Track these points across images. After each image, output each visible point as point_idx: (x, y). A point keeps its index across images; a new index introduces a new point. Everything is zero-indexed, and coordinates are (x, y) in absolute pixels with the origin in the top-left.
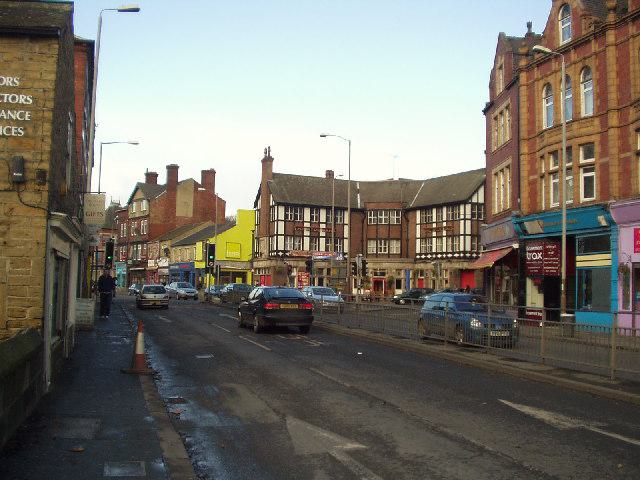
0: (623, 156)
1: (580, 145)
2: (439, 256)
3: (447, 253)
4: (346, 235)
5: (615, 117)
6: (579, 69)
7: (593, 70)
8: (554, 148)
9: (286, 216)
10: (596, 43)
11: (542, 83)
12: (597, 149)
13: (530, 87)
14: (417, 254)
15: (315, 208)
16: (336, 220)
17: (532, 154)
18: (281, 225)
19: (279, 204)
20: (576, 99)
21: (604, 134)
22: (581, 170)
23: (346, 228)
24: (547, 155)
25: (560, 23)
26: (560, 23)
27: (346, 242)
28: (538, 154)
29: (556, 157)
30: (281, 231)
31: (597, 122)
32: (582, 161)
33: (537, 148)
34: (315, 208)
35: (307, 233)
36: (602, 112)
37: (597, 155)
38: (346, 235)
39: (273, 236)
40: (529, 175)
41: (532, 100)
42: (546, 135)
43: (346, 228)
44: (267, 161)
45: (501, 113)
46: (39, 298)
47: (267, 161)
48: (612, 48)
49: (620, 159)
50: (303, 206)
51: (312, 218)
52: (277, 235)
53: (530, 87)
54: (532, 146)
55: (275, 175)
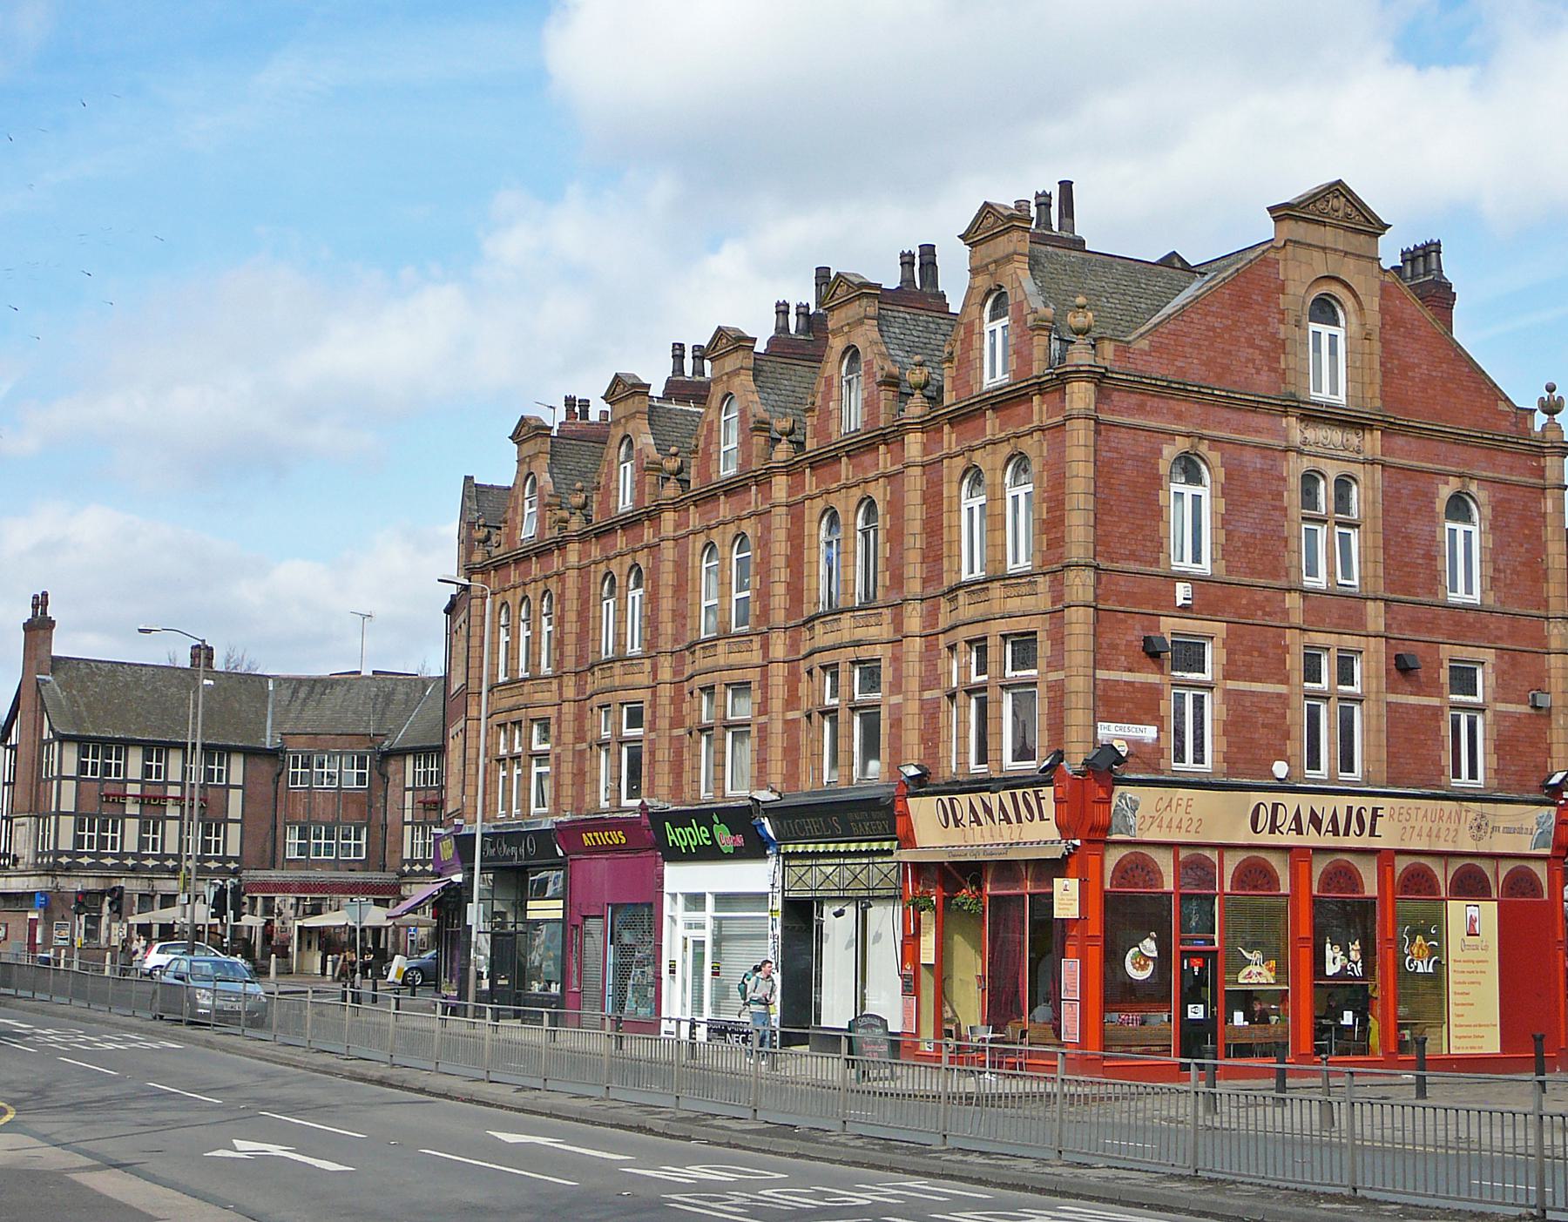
0: (927, 695)
1: (1004, 637)
2: (418, 868)
3: (424, 862)
4: (235, 810)
5: (572, 683)
6: (855, 501)
7: (1035, 467)
8: (975, 631)
9: (82, 767)
10: (596, 545)
11: (819, 504)
12: (1044, 648)
13: (795, 509)
14: (404, 862)
15: (155, 749)
16: (209, 774)
17: (929, 637)
18: (69, 788)
19: (63, 739)
20: (993, 519)
21: (1056, 615)
22: (534, 762)
23: (236, 797)
24: (962, 646)
25: (527, 503)
26: (527, 503)
27: (234, 831)
28: (943, 641)
29: (545, 728)
30: (68, 804)
31: (1043, 583)
32: (536, 747)
33: (803, 652)
34: (155, 749)
35: (132, 809)
36: (1054, 566)
37: (1041, 662)
38: (235, 810)
39: (47, 816)
40: (923, 689)
41: (934, 499)
42: (962, 596)
43: (236, 797)
44: (39, 626)
45: (460, 627)
46: (1524, 457)
47: (39, 626)
48: (918, 471)
49: (786, 722)
50: (126, 744)
51: (147, 771)
52: (59, 813)
53: (795, 509)
54: (932, 616)
55: (58, 663)
